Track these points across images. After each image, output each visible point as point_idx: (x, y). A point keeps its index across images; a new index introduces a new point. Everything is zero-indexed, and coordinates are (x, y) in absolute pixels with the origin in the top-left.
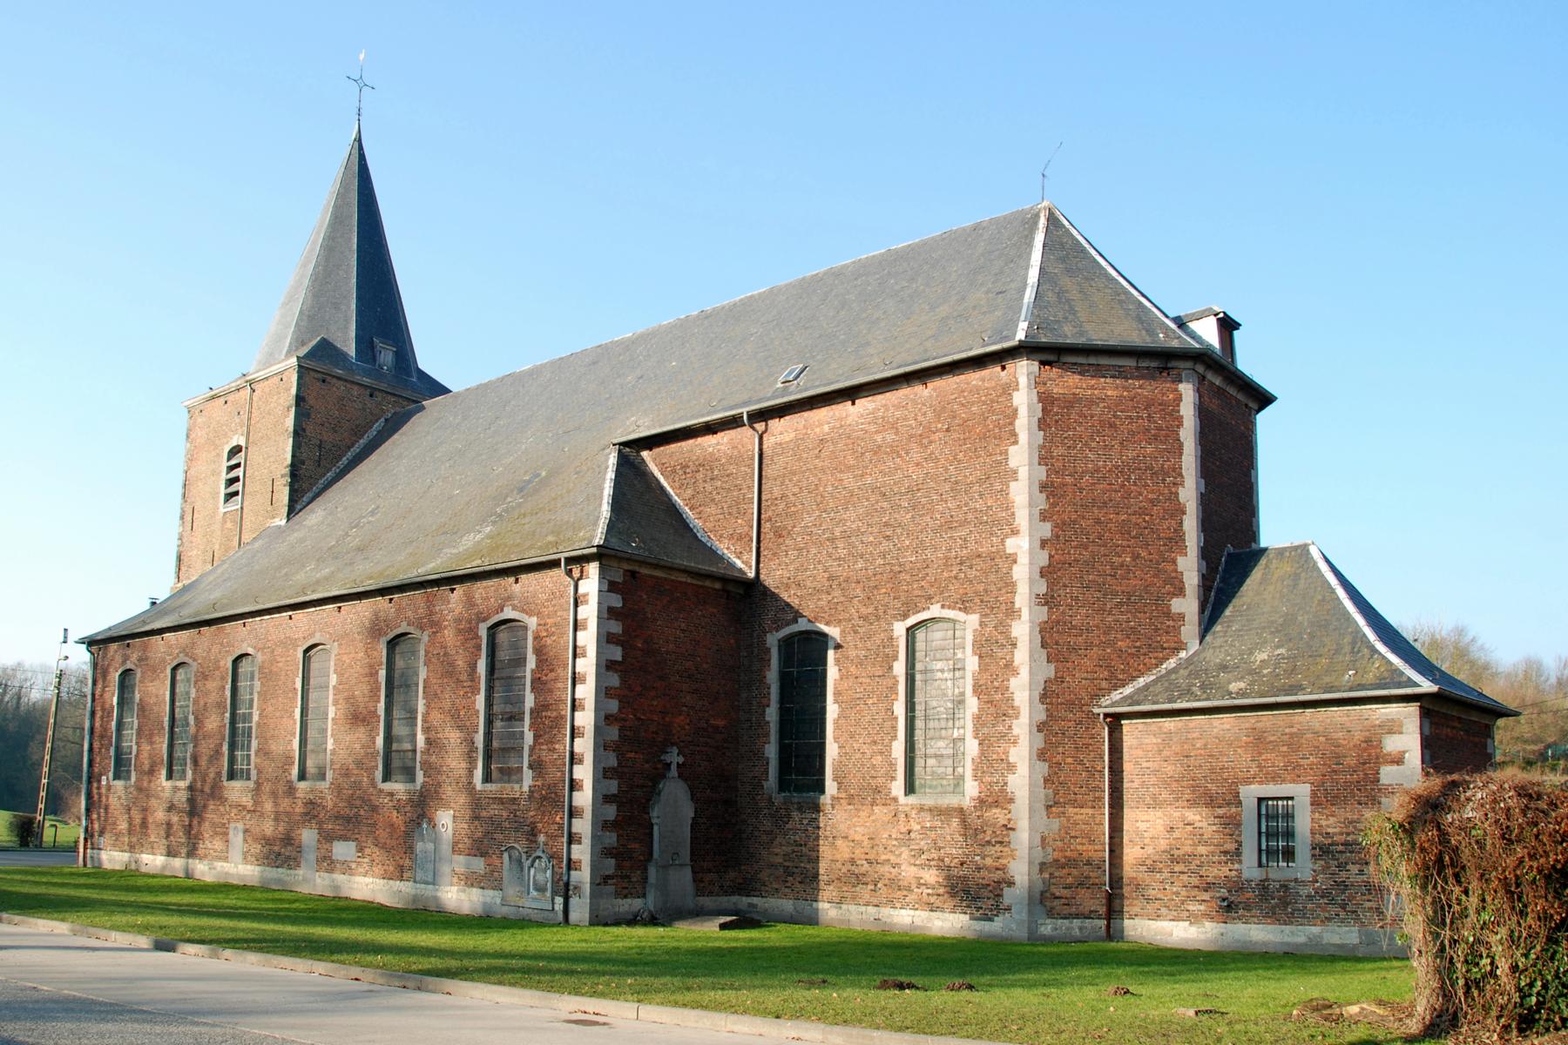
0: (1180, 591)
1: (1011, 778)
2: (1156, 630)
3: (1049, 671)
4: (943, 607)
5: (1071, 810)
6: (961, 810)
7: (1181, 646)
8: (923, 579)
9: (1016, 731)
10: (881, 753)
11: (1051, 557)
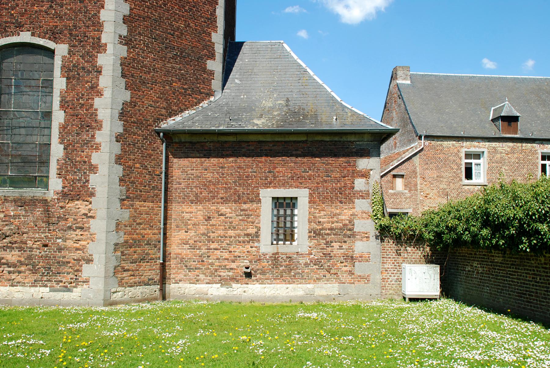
0: (212, 56)
1: (92, 177)
2: (197, 79)
3: (127, 96)
5: (137, 203)
6: (45, 202)
7: (210, 94)
8: (13, 8)
9: (98, 139)
11: (131, 9)
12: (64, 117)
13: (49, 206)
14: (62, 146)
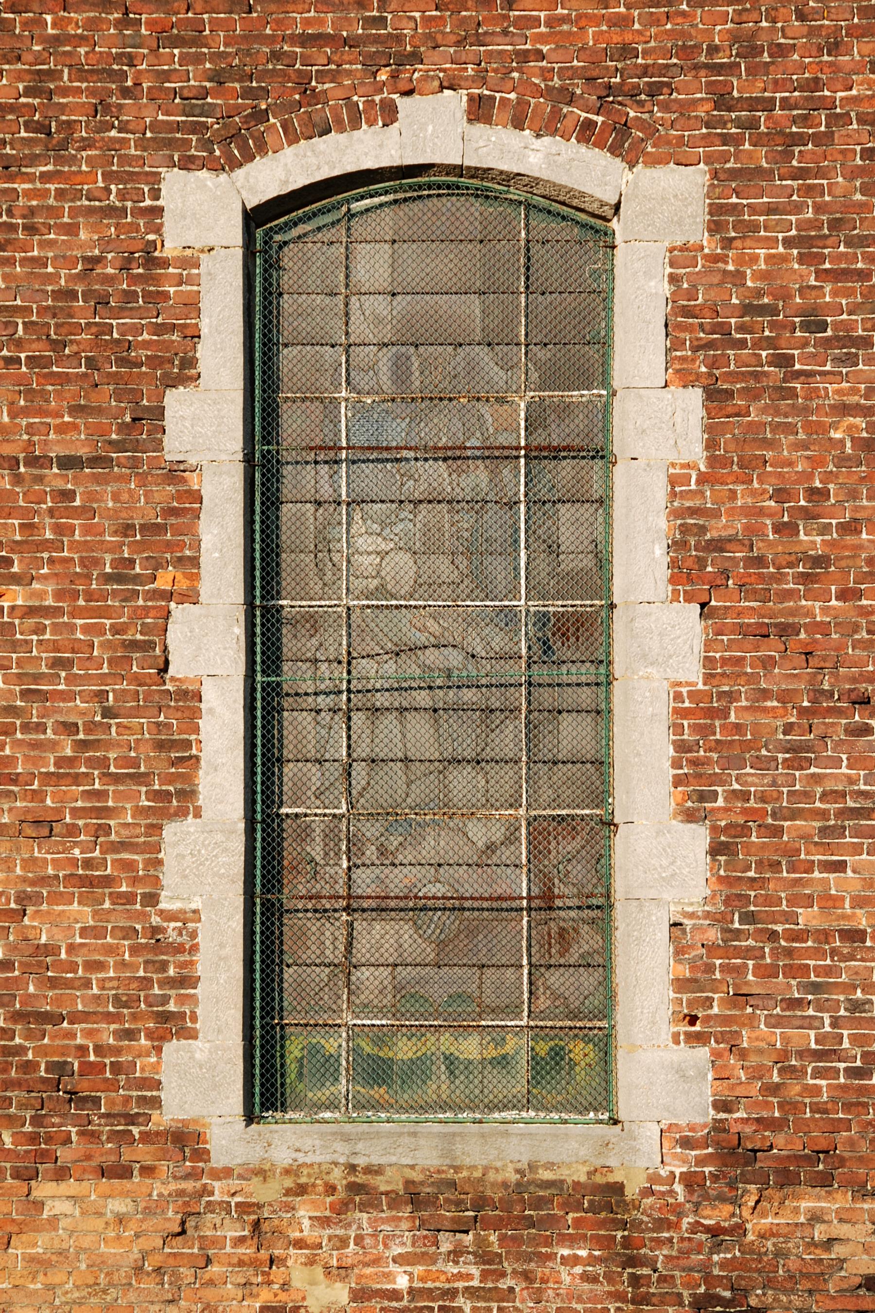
4: (480, 111)
6: (607, 1198)
10: (90, 884)
12: (698, 645)
13: (637, 1225)
14: (699, 837)
